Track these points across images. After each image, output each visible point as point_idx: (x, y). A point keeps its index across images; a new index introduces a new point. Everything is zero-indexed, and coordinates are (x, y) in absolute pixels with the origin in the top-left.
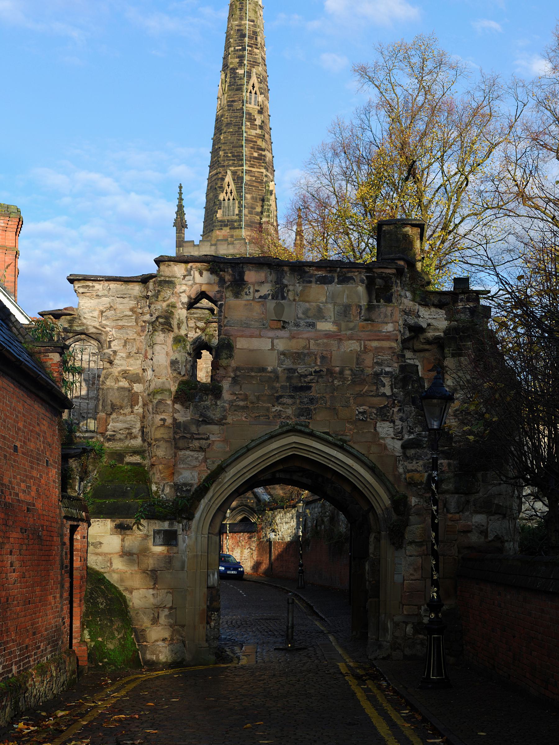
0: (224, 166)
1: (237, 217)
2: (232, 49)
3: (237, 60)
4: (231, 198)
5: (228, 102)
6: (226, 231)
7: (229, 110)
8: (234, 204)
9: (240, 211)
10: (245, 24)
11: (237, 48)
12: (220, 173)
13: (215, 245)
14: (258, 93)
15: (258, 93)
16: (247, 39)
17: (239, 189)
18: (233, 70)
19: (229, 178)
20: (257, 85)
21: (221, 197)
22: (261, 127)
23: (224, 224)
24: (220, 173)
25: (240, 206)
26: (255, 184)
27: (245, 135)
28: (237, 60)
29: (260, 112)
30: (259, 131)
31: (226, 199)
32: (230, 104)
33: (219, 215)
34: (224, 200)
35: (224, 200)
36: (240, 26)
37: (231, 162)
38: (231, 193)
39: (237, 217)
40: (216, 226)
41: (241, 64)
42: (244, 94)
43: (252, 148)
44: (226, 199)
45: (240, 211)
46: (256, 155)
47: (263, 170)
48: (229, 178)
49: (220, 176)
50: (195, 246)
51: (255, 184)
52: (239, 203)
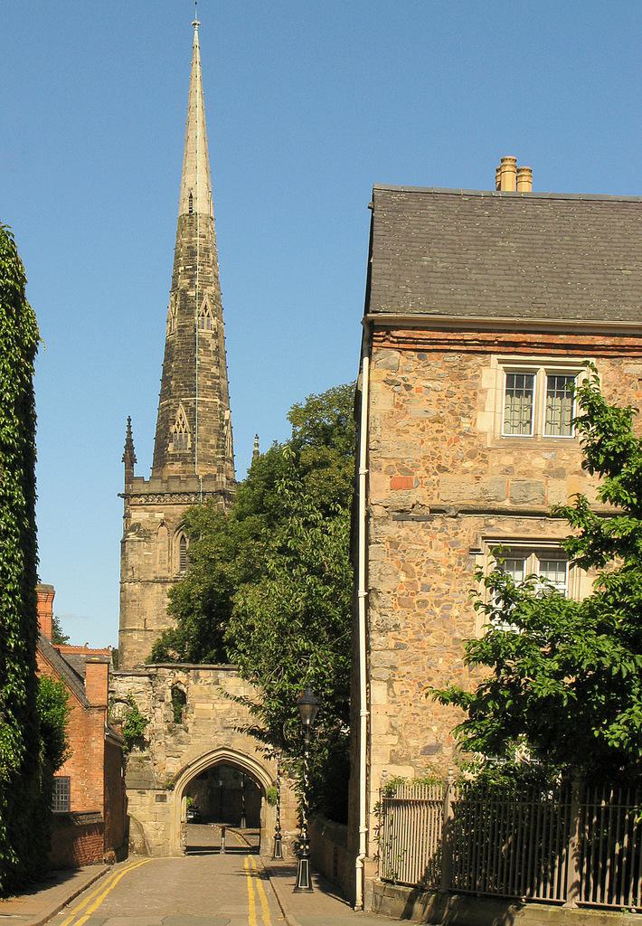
0: (175, 397)
1: (189, 452)
2: (183, 268)
3: (188, 281)
4: (183, 430)
5: (179, 326)
6: (177, 466)
7: (180, 336)
8: (186, 437)
9: (193, 445)
10: (196, 241)
11: (187, 267)
12: (171, 404)
13: (166, 482)
14: (211, 315)
15: (211, 315)
16: (198, 257)
17: (192, 422)
18: (184, 292)
19: (181, 411)
20: (209, 307)
21: (172, 430)
22: (216, 353)
23: (175, 458)
24: (171, 404)
25: (193, 440)
26: (209, 415)
27: (198, 362)
28: (188, 281)
29: (216, 336)
30: (213, 358)
31: (178, 431)
32: (181, 330)
33: (170, 449)
34: (176, 432)
35: (176, 432)
36: (190, 243)
37: (183, 393)
38: (183, 425)
39: (189, 452)
40: (167, 461)
41: (192, 285)
42: (196, 318)
43: (205, 376)
44: (178, 431)
45: (193, 445)
46: (209, 383)
47: (218, 400)
48: (181, 411)
49: (172, 407)
50: (145, 482)
51: (209, 415)
52: (192, 436)
